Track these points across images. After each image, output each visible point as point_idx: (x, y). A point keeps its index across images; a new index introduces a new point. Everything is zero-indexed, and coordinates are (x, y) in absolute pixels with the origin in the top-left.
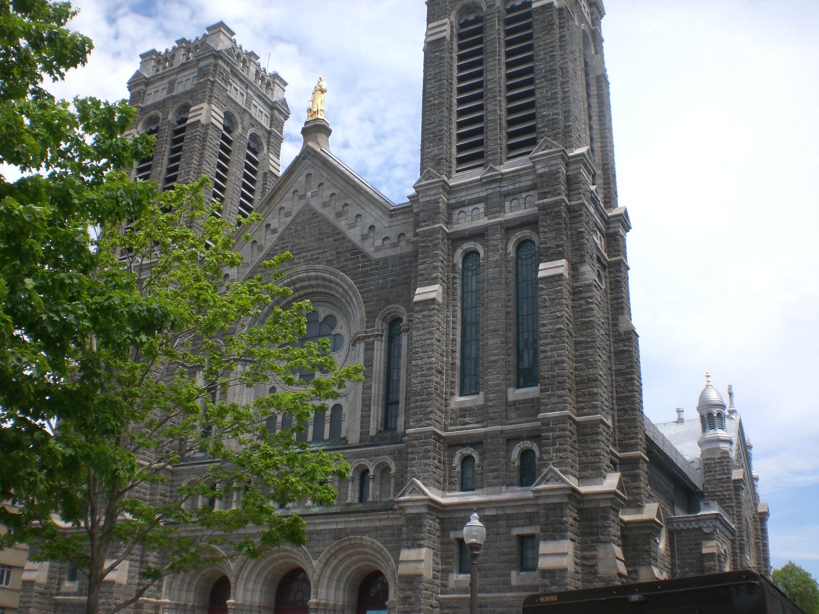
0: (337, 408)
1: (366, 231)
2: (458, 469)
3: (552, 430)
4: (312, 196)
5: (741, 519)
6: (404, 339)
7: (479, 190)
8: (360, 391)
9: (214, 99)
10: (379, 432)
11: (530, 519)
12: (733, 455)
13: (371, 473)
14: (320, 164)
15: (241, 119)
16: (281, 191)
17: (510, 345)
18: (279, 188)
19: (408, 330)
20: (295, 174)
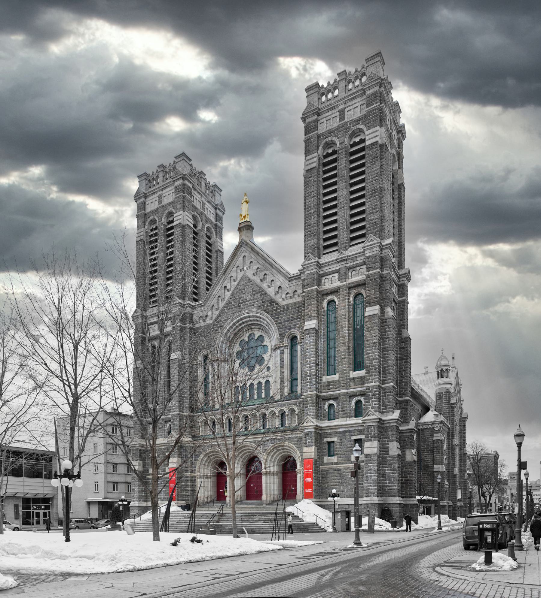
0: (267, 382)
1: (277, 289)
2: (327, 410)
3: (371, 392)
4: (247, 269)
5: (453, 422)
6: (299, 348)
7: (335, 265)
8: (279, 374)
9: (186, 208)
10: (289, 394)
11: (360, 432)
12: (452, 391)
13: (287, 413)
14: (250, 250)
15: (201, 218)
16: (230, 267)
17: (351, 350)
18: (229, 265)
19: (301, 343)
20: (237, 256)
